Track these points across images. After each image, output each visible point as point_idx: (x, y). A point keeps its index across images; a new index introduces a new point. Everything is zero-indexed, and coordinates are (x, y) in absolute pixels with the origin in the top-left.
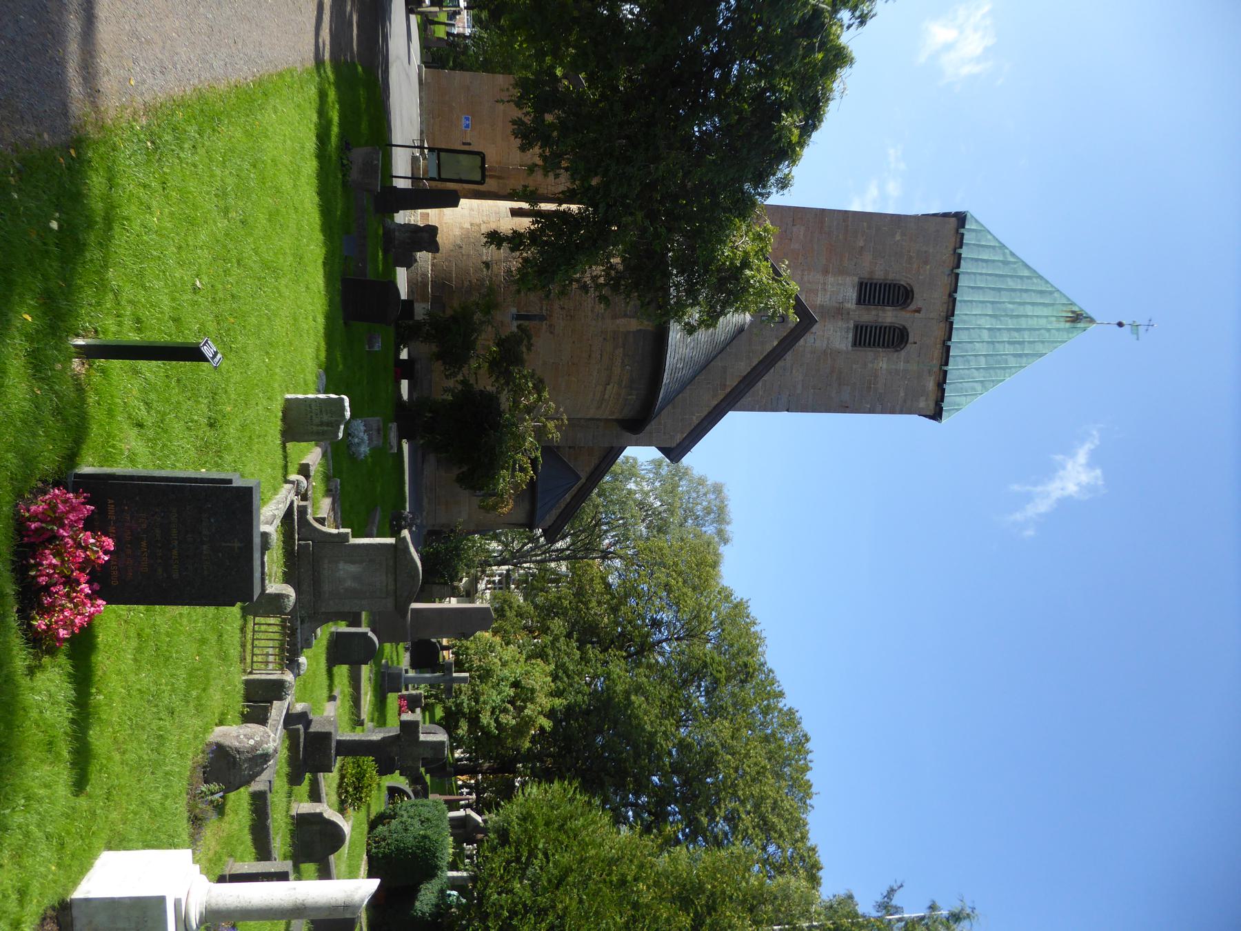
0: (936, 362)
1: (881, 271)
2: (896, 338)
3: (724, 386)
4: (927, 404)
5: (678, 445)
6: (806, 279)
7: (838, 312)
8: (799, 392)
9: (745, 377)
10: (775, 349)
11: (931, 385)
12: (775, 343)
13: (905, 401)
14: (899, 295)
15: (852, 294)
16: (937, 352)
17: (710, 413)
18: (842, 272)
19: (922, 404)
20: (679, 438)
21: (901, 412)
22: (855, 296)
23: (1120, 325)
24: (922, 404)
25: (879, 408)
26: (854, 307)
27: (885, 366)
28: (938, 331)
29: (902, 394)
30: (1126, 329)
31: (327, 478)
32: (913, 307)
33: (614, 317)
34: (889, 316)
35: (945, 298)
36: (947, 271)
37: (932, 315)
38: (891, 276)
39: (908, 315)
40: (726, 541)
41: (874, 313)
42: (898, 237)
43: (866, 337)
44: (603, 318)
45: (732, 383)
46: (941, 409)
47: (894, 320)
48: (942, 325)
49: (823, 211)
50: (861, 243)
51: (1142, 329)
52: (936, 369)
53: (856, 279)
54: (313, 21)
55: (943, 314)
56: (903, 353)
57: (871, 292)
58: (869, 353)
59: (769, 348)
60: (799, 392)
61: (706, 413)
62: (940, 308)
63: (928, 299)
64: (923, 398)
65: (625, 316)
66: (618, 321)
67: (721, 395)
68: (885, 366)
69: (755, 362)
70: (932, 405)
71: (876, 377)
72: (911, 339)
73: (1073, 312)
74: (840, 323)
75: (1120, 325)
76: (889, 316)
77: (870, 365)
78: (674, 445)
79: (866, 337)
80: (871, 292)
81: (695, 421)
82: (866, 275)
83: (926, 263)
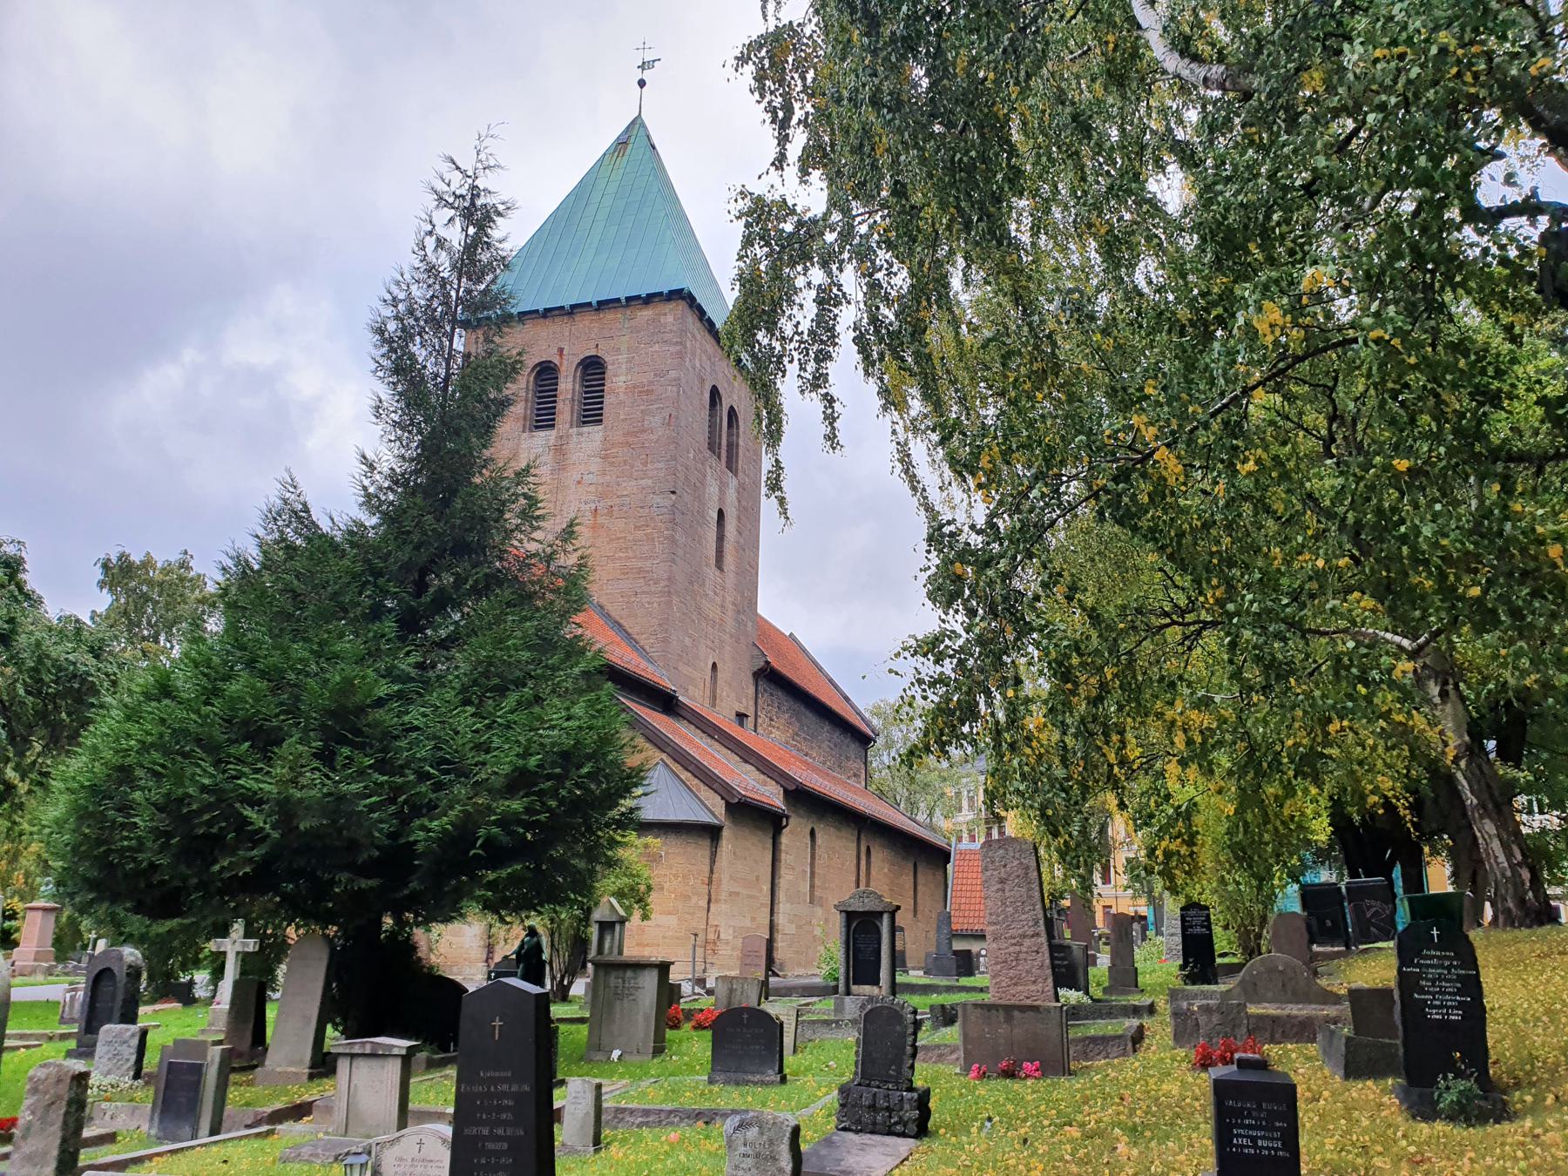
2: (593, 368)
7: (559, 450)
28: (584, 322)
29: (656, 347)
34: (568, 385)
43: (591, 413)
56: (608, 358)
68: (623, 378)
70: (672, 305)
72: (593, 352)
75: (642, 83)
76: (568, 385)
79: (591, 413)
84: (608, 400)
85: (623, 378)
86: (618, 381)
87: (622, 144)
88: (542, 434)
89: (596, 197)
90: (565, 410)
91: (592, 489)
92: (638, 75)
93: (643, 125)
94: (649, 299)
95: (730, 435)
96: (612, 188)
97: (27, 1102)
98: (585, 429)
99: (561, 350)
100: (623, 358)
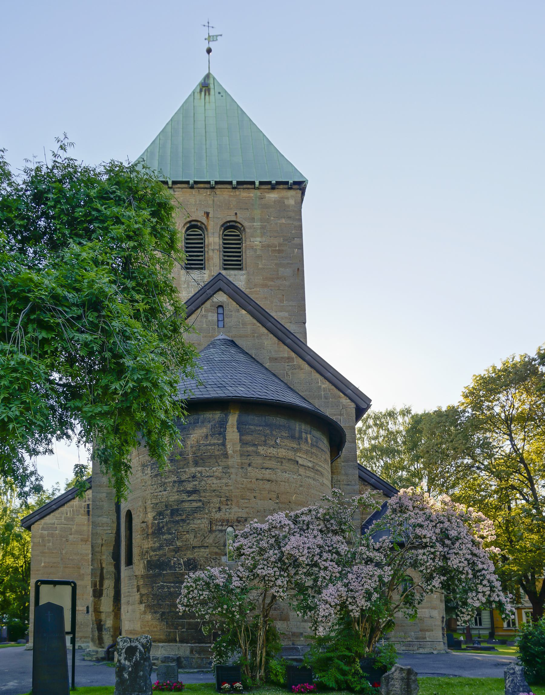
0: (253, 194)
3: (290, 359)
4: (291, 196)
10: (249, 312)
11: (273, 196)
12: (244, 312)
13: (290, 218)
16: (243, 194)
19: (292, 202)
20: (345, 401)
21: (300, 220)
22: (197, 272)
23: (209, 51)
24: (292, 202)
25: (296, 241)
26: (207, 272)
27: (259, 239)
28: (224, 194)
29: (283, 221)
30: (212, 45)
32: (204, 220)
33: (226, 455)
34: (214, 240)
37: (211, 202)
40: (409, 411)
41: (211, 253)
44: (228, 467)
45: (286, 352)
46: (295, 183)
47: (217, 235)
48: (218, 192)
51: (213, 32)
52: (258, 192)
54: (495, 619)
55: (209, 191)
56: (246, 224)
58: (248, 256)
61: (318, 376)
62: (203, 196)
64: (286, 202)
65: (224, 444)
66: (230, 452)
67: (298, 361)
69: (263, 330)
70: (291, 193)
71: (269, 246)
72: (234, 219)
73: (201, 91)
75: (209, 51)
76: (214, 240)
77: (259, 253)
78: (353, 405)
81: (326, 385)
99: (207, 214)
100: (257, 224)
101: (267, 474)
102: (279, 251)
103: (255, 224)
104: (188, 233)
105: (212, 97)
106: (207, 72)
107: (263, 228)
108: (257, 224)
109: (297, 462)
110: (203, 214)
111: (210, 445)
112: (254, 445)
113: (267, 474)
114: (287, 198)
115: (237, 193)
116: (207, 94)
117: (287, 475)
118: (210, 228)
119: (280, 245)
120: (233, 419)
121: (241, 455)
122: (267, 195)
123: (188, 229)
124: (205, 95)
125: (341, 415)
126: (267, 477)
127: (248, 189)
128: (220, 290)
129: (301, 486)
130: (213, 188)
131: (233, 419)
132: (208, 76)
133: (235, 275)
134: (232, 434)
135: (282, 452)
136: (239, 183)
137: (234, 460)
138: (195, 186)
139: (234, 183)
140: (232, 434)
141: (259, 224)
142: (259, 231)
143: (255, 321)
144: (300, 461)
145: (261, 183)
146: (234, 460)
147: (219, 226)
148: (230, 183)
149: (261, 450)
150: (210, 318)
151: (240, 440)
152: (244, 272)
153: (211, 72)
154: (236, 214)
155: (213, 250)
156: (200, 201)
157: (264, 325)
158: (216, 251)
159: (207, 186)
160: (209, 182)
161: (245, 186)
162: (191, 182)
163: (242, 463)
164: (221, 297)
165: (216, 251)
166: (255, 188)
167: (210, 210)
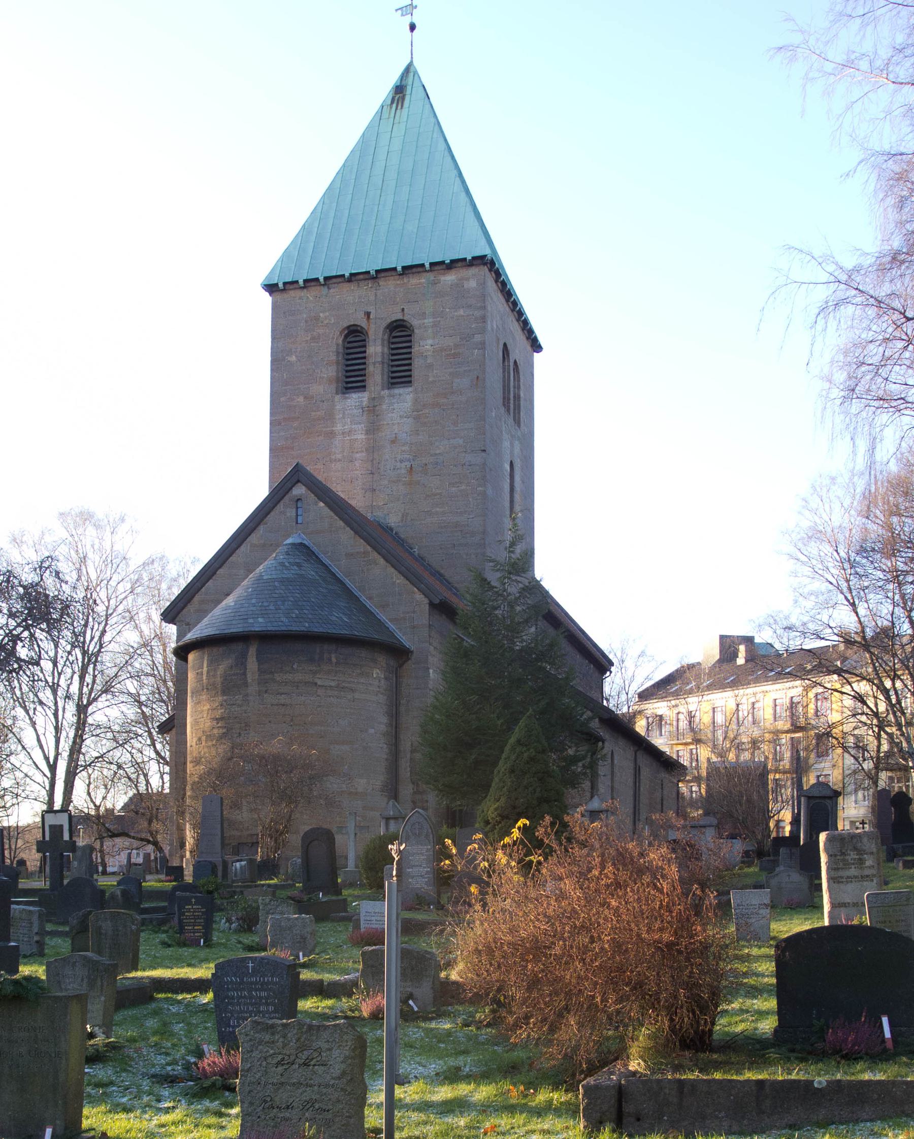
1: (329, 370)
2: (400, 331)
5: (426, 596)
6: (339, 456)
7: (373, 411)
8: (461, 441)
9: (356, 532)
11: (450, 278)
12: (322, 504)
14: (354, 337)
15: (356, 399)
17: (393, 566)
18: (330, 417)
23: (413, 27)
28: (389, 285)
29: (461, 312)
31: (787, 1080)
32: (364, 323)
33: (246, 684)
34: (376, 350)
35: (353, 286)
36: (324, 290)
37: (372, 298)
38: (333, 358)
39: (373, 326)
42: (294, 358)
43: (400, 373)
46: (474, 258)
47: (379, 342)
49: (272, 450)
50: (301, 399)
52: (431, 276)
53: (337, 398)
56: (415, 322)
57: (352, 378)
59: (327, 511)
60: (461, 441)
61: (393, 570)
63: (353, 305)
65: (245, 674)
66: (249, 681)
68: (430, 342)
69: (341, 523)
70: (473, 271)
72: (399, 316)
74: (384, 407)
75: (413, 27)
76: (376, 350)
79: (400, 373)
80: (352, 378)
82: (333, 386)
83: (317, 318)
84: (417, 363)
85: (430, 342)
86: (425, 345)
87: (400, 91)
88: (354, 396)
89: (381, 155)
90: (376, 373)
91: (406, 448)
92: (407, 20)
93: (416, 73)
94: (453, 264)
95: (799, 813)
96: (397, 145)
97: (464, 1017)
98: (397, 391)
99: (368, 314)
100: (428, 321)
101: (283, 699)
102: (455, 356)
103: (426, 321)
104: (349, 340)
105: (405, 110)
106: (409, 61)
107: (435, 325)
108: (428, 321)
109: (316, 684)
110: (363, 316)
111: (234, 675)
112: (272, 673)
113: (283, 699)
114: (468, 279)
115: (405, 280)
116: (399, 107)
117: (303, 698)
118: (371, 333)
119: (456, 346)
120: (252, 650)
121: (259, 684)
122: (443, 278)
123: (346, 336)
124: (396, 109)
125: (414, 612)
126: (282, 702)
127: (419, 272)
128: (298, 481)
129: (320, 706)
130: (373, 278)
131: (252, 650)
132: (409, 70)
133: (400, 395)
134: (252, 664)
135: (298, 677)
136: (404, 268)
137: (253, 689)
138: (353, 278)
139: (399, 269)
140: (252, 664)
141: (431, 320)
142: (430, 331)
143: (332, 514)
144: (319, 682)
145: (432, 264)
146: (253, 689)
147: (382, 329)
148: (395, 269)
149: (278, 677)
150: (288, 514)
151: (259, 670)
152: (410, 389)
153: (415, 63)
154: (403, 310)
155: (374, 364)
156: (359, 298)
157: (341, 519)
158: (377, 365)
159: (366, 276)
160: (368, 272)
161: (414, 270)
162: (347, 275)
163: (259, 691)
164: (299, 490)
165: (377, 365)
166: (426, 271)
167: (371, 309)
